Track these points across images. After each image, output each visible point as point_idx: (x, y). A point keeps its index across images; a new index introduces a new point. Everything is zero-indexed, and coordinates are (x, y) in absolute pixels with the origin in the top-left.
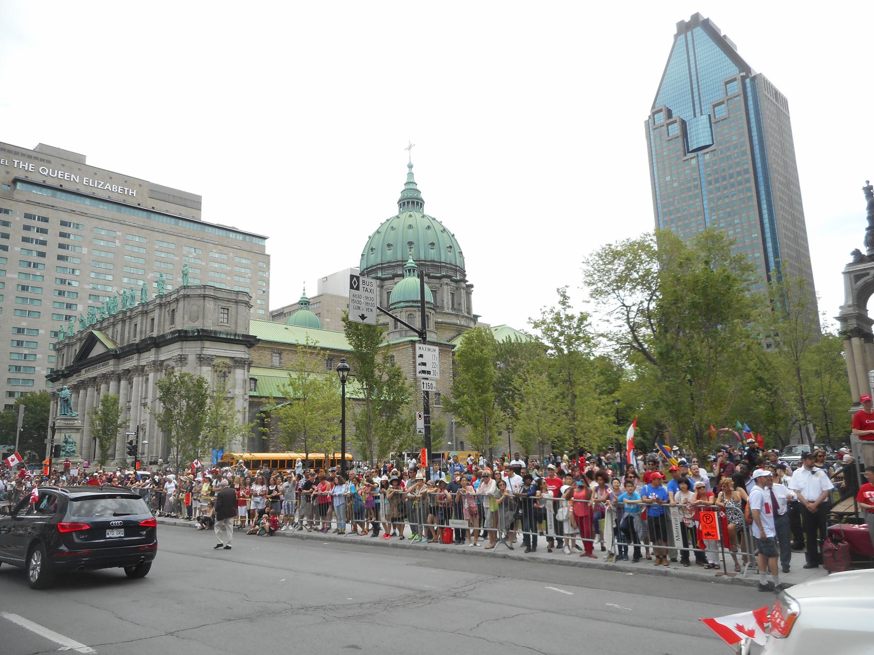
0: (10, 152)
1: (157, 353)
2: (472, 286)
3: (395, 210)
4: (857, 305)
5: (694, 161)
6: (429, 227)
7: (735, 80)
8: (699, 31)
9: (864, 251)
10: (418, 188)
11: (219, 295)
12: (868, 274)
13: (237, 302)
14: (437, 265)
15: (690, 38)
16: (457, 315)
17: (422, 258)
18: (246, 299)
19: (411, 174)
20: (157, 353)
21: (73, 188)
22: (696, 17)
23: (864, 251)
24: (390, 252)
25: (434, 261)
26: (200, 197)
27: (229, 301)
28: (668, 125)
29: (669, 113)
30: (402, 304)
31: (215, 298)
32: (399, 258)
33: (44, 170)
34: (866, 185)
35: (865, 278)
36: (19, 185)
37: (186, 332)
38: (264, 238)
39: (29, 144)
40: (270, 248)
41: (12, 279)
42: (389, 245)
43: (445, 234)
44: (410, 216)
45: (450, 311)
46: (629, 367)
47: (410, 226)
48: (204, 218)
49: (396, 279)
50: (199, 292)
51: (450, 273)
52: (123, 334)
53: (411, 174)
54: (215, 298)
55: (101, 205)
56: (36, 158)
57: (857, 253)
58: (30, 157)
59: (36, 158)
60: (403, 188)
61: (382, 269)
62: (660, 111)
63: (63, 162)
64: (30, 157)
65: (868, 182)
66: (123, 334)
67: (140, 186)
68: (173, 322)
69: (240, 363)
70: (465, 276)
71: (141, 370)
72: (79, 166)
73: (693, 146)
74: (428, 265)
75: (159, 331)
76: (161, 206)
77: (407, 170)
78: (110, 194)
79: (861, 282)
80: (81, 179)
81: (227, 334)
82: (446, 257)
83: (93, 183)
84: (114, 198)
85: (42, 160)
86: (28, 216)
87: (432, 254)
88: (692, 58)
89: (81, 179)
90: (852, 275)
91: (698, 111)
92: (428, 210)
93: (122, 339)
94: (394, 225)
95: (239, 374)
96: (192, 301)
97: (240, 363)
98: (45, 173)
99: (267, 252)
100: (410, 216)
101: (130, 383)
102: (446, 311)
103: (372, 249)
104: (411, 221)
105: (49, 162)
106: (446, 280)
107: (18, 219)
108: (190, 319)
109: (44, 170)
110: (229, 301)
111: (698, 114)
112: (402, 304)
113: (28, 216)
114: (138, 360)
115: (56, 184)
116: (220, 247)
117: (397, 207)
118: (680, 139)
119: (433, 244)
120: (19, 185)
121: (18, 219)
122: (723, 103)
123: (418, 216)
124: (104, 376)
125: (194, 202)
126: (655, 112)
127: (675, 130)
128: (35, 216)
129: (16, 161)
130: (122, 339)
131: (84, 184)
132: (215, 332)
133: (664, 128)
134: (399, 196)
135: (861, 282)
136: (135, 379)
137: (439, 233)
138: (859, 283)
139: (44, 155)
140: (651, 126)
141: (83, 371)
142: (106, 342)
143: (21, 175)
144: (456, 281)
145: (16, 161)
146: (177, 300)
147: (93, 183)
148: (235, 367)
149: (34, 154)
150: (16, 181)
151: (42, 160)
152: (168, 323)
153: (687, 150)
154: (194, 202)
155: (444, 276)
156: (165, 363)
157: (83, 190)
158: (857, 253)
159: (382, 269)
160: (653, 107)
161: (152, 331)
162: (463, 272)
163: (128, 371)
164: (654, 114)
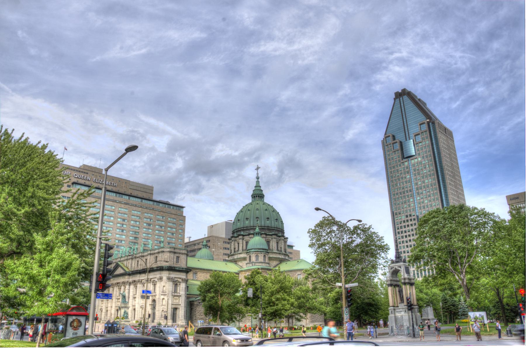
2: (287, 238)
3: (249, 200)
5: (406, 164)
6: (266, 210)
7: (424, 123)
8: (406, 98)
10: (262, 188)
14: (269, 229)
15: (401, 100)
16: (280, 254)
17: (263, 225)
19: (258, 182)
24: (247, 222)
28: (393, 144)
29: (394, 138)
30: (253, 250)
32: (252, 225)
37: (163, 267)
38: (183, 207)
40: (186, 212)
42: (247, 219)
44: (257, 204)
45: (276, 251)
47: (257, 209)
49: (251, 236)
51: (276, 233)
52: (131, 265)
53: (258, 182)
60: (254, 188)
61: (243, 230)
62: (389, 136)
63: (94, 173)
66: (131, 265)
70: (284, 233)
72: (100, 175)
73: (405, 157)
77: (256, 180)
82: (274, 224)
87: (268, 223)
88: (403, 110)
91: (407, 137)
92: (266, 200)
93: (131, 267)
94: (249, 208)
96: (165, 254)
100: (257, 204)
102: (274, 251)
103: (239, 220)
104: (257, 206)
106: (274, 236)
111: (408, 139)
112: (253, 250)
116: (162, 213)
118: (400, 152)
119: (268, 218)
122: (419, 134)
123: (261, 203)
124: (124, 283)
126: (386, 137)
127: (397, 146)
130: (131, 267)
133: (392, 145)
134: (252, 193)
137: (271, 212)
140: (385, 144)
142: (288, 339)
144: (279, 236)
146: (159, 253)
153: (403, 158)
155: (273, 234)
156: (152, 280)
159: (243, 230)
160: (385, 134)
162: (282, 231)
164: (386, 137)
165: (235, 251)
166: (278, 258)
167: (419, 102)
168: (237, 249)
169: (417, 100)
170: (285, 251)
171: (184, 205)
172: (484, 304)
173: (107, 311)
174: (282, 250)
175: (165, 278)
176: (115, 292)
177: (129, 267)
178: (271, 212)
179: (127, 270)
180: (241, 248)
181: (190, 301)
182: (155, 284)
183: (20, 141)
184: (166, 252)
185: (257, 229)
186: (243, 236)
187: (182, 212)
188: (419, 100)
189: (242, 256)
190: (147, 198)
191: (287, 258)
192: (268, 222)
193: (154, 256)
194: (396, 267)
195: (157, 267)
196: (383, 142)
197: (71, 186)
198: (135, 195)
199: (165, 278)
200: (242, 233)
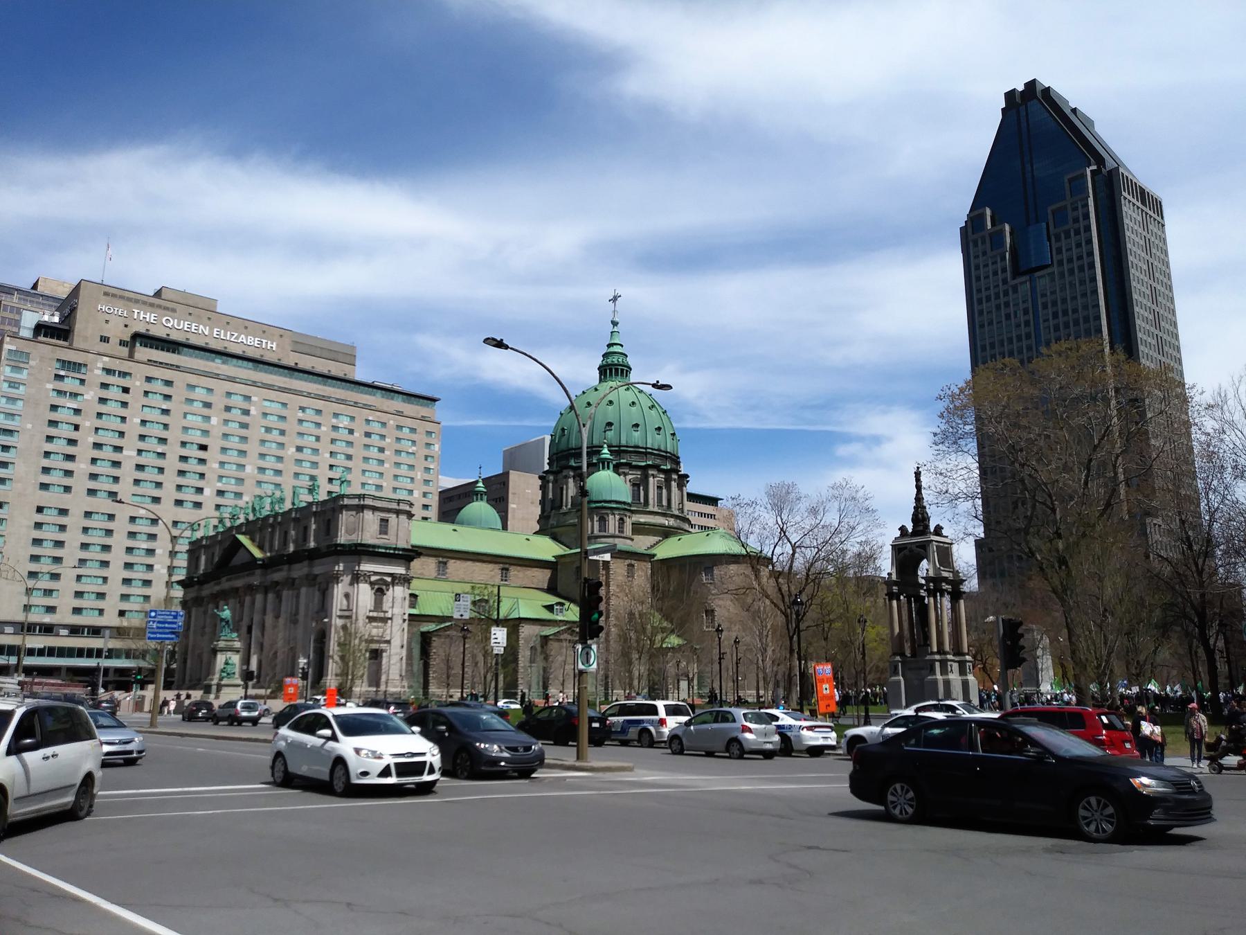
1: (311, 566)
11: (378, 504)
13: (398, 512)
15: (1023, 113)
17: (623, 442)
18: (407, 508)
20: (311, 566)
22: (1031, 85)
23: (910, 529)
27: (389, 511)
31: (374, 509)
36: (142, 353)
41: (130, 457)
43: (653, 412)
45: (656, 509)
50: (356, 502)
51: (658, 462)
54: (374, 509)
63: (191, 310)
69: (397, 580)
70: (678, 463)
71: (291, 583)
76: (306, 362)
78: (245, 348)
81: (386, 548)
84: (250, 353)
85: (166, 308)
87: (636, 438)
95: (399, 592)
97: (397, 580)
101: (279, 597)
102: (651, 508)
105: (174, 310)
107: (138, 383)
108: (347, 532)
110: (389, 511)
114: (289, 570)
117: (596, 374)
119: (637, 425)
121: (138, 383)
132: (374, 546)
136: (285, 593)
137: (646, 409)
141: (224, 579)
148: (393, 584)
150: (136, 336)
151: (166, 308)
158: (903, 529)
163: (277, 583)
166: (662, 526)
167: (1072, 117)
169: (1068, 112)
170: (682, 510)
171: (436, 396)
172: (1058, 685)
178: (646, 409)
181: (423, 634)
185: (606, 451)
188: (1074, 111)
190: (341, 375)
191: (686, 527)
192: (636, 434)
196: (964, 232)
198: (308, 367)
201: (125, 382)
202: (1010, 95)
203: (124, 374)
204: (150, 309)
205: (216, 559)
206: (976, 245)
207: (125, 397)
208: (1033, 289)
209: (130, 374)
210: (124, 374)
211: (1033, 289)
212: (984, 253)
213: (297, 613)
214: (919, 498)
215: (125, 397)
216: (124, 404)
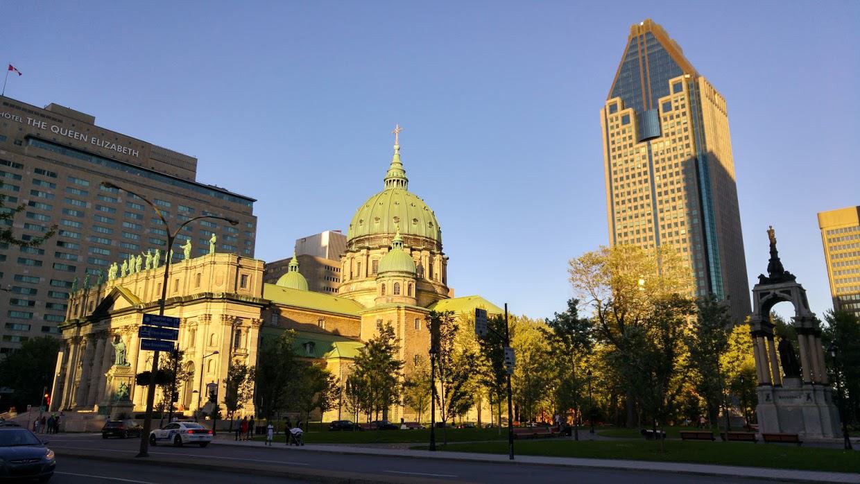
0: (25, 110)
4: (762, 314)
9: (767, 275)
12: (769, 293)
21: (81, 146)
23: (767, 275)
24: (377, 225)
25: (416, 235)
26: (196, 160)
33: (55, 129)
34: (769, 229)
35: (768, 296)
38: (253, 201)
39: (41, 102)
40: (257, 210)
41: (19, 229)
42: (377, 219)
43: (396, 207)
46: (551, 392)
48: (199, 179)
55: (104, 163)
56: (48, 117)
57: (762, 277)
58: (43, 116)
59: (48, 117)
63: (74, 122)
64: (43, 116)
65: (770, 227)
67: (143, 147)
68: (198, 284)
74: (411, 239)
75: (184, 292)
76: (160, 167)
79: (765, 298)
80: (89, 139)
83: (100, 143)
84: (118, 158)
86: (38, 171)
87: (414, 229)
89: (89, 139)
90: (759, 293)
98: (56, 132)
99: (254, 214)
103: (361, 221)
105: (60, 121)
109: (55, 129)
113: (38, 171)
115: (65, 142)
120: (31, 141)
121: (29, 173)
125: (191, 163)
128: (44, 171)
129: (30, 119)
131: (93, 143)
135: (765, 298)
138: (763, 299)
139: (56, 114)
143: (34, 133)
145: (30, 119)
147: (100, 143)
149: (43, 112)
150: (28, 137)
152: (193, 285)
154: (191, 163)
156: (189, 320)
157: (90, 149)
158: (762, 277)
161: (177, 290)
165: (351, 278)
168: (355, 274)
173: (89, 387)
174: (439, 279)
175: (216, 318)
176: (17, 335)
177: (141, 297)
179: (135, 302)
180: (363, 272)
182: (194, 331)
183: (125, 261)
184: (221, 263)
186: (369, 249)
187: (251, 209)
189: (367, 285)
193: (193, 272)
194: (777, 292)
195: (200, 295)
197: (24, 143)
199: (216, 318)
200: (367, 244)
201: (19, 172)
202: (795, 278)
203: (18, 166)
204: (42, 118)
205: (99, 304)
206: (612, 121)
207: (17, 183)
208: (650, 151)
209: (22, 166)
210: (18, 166)
211: (650, 151)
212: (617, 126)
213: (92, 359)
214: (774, 252)
215: (17, 183)
216: (17, 188)
